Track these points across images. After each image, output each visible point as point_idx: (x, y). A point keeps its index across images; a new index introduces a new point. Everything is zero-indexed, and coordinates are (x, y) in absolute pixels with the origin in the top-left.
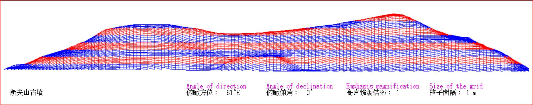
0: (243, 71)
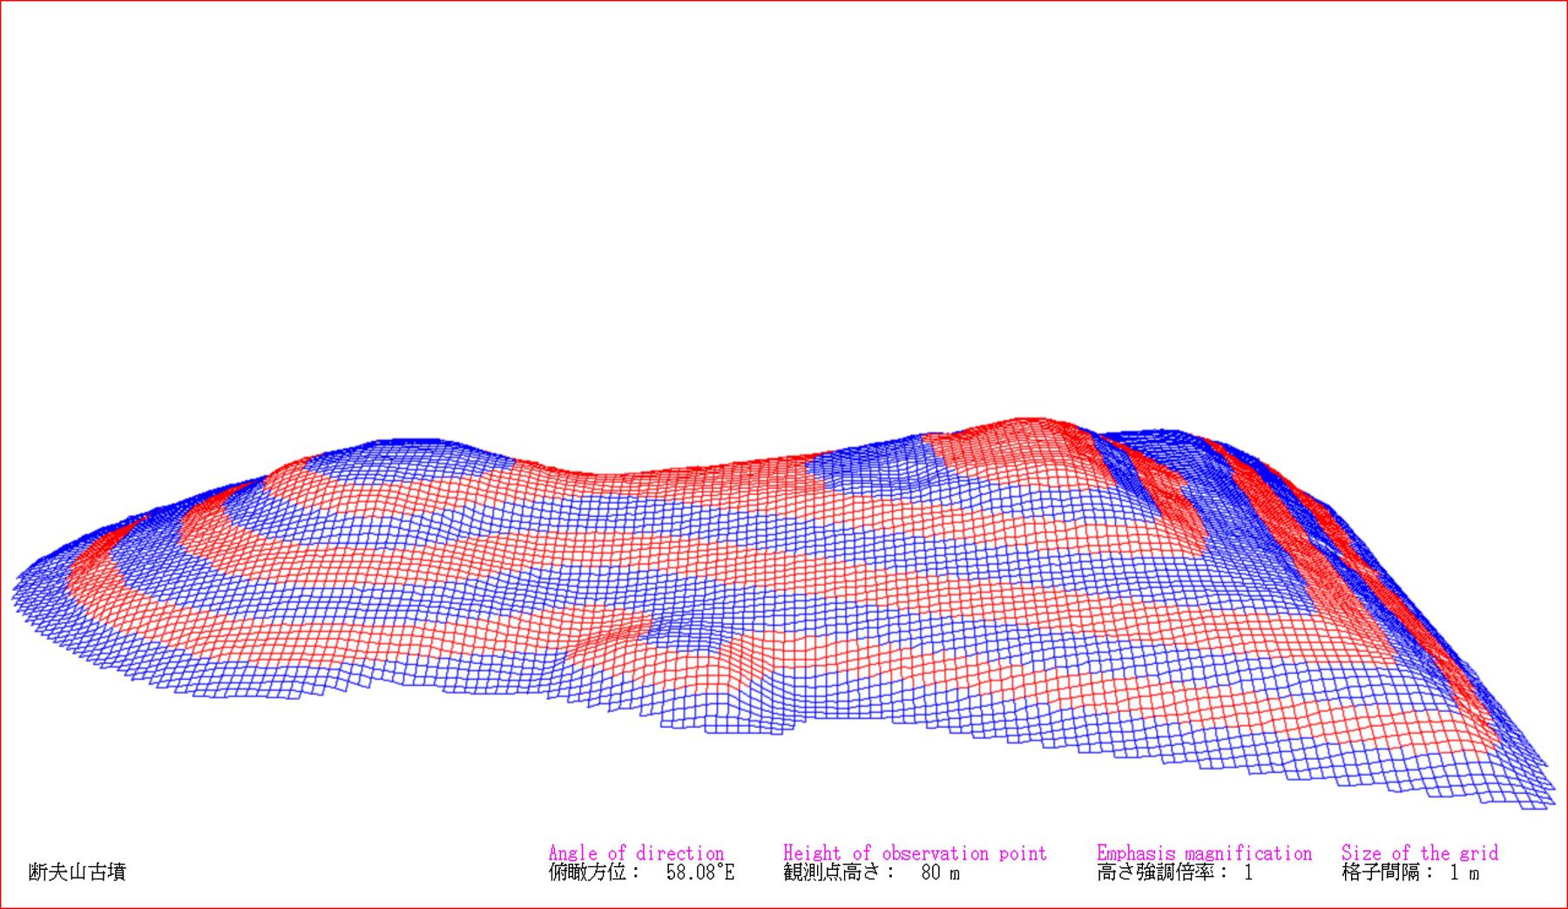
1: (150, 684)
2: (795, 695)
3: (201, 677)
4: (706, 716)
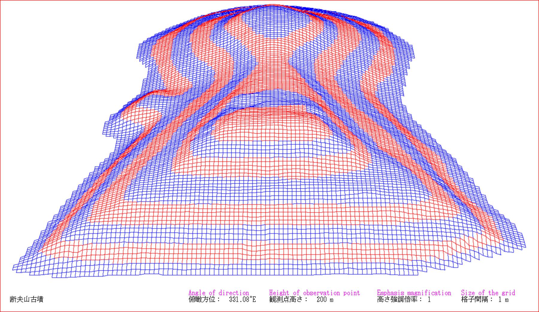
0: (461, 165)
2: (312, 124)
4: (201, 166)
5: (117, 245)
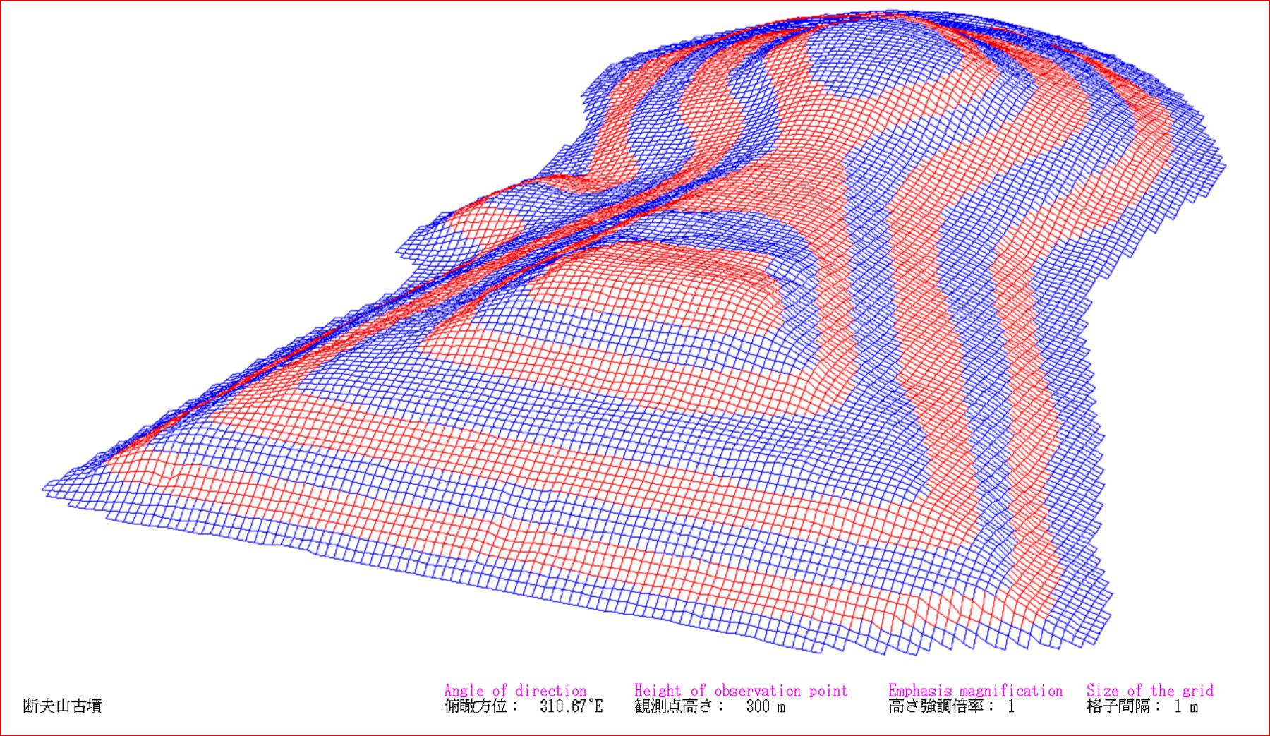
1: (413, 264)
3: (813, 105)
5: (220, 474)
